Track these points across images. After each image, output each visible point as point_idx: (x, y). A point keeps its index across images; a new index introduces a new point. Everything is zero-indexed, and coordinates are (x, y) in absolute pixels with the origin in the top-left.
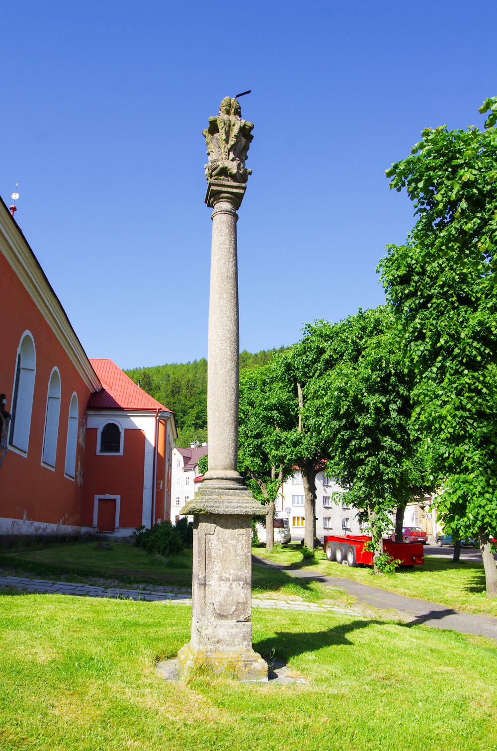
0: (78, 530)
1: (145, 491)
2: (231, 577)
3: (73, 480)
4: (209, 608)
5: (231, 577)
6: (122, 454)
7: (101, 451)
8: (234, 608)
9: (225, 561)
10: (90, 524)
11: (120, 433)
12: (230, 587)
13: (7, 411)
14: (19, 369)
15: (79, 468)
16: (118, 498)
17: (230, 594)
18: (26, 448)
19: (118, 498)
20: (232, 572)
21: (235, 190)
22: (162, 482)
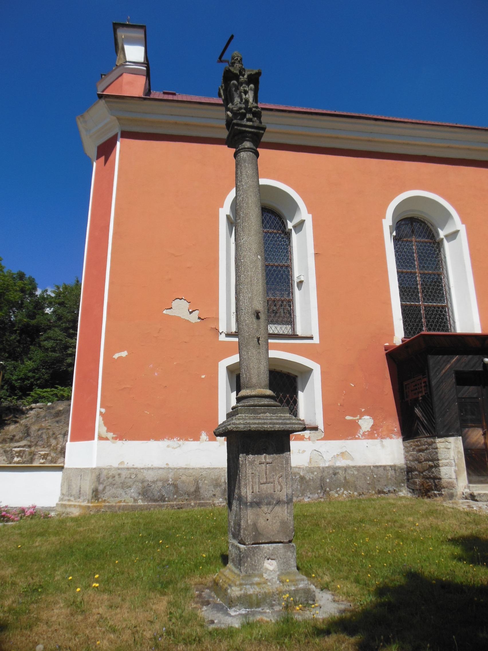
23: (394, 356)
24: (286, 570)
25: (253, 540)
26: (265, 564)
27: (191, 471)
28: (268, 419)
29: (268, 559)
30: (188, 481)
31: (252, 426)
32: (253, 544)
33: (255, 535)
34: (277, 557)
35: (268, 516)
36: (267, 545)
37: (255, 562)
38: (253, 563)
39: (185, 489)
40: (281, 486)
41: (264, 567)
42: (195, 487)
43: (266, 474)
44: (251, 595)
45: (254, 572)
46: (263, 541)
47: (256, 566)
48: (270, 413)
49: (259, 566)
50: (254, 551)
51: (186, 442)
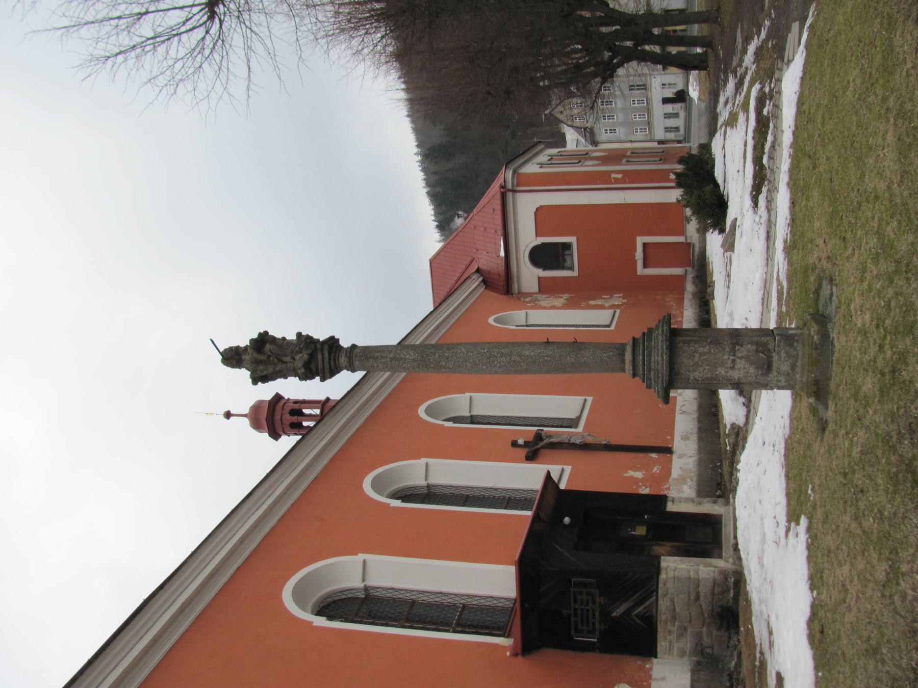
0: (690, 296)
1: (629, 201)
2: (732, 358)
3: (618, 311)
4: (761, 379)
5: (732, 358)
6: (575, 238)
7: (571, 268)
8: (761, 354)
9: (715, 363)
10: (682, 279)
11: (543, 244)
12: (741, 358)
13: (533, 435)
14: (473, 420)
15: (599, 302)
16: (640, 240)
17: (747, 358)
18: (580, 399)
19: (640, 240)
20: (726, 357)
21: (326, 355)
22: (613, 176)
23: (527, 647)
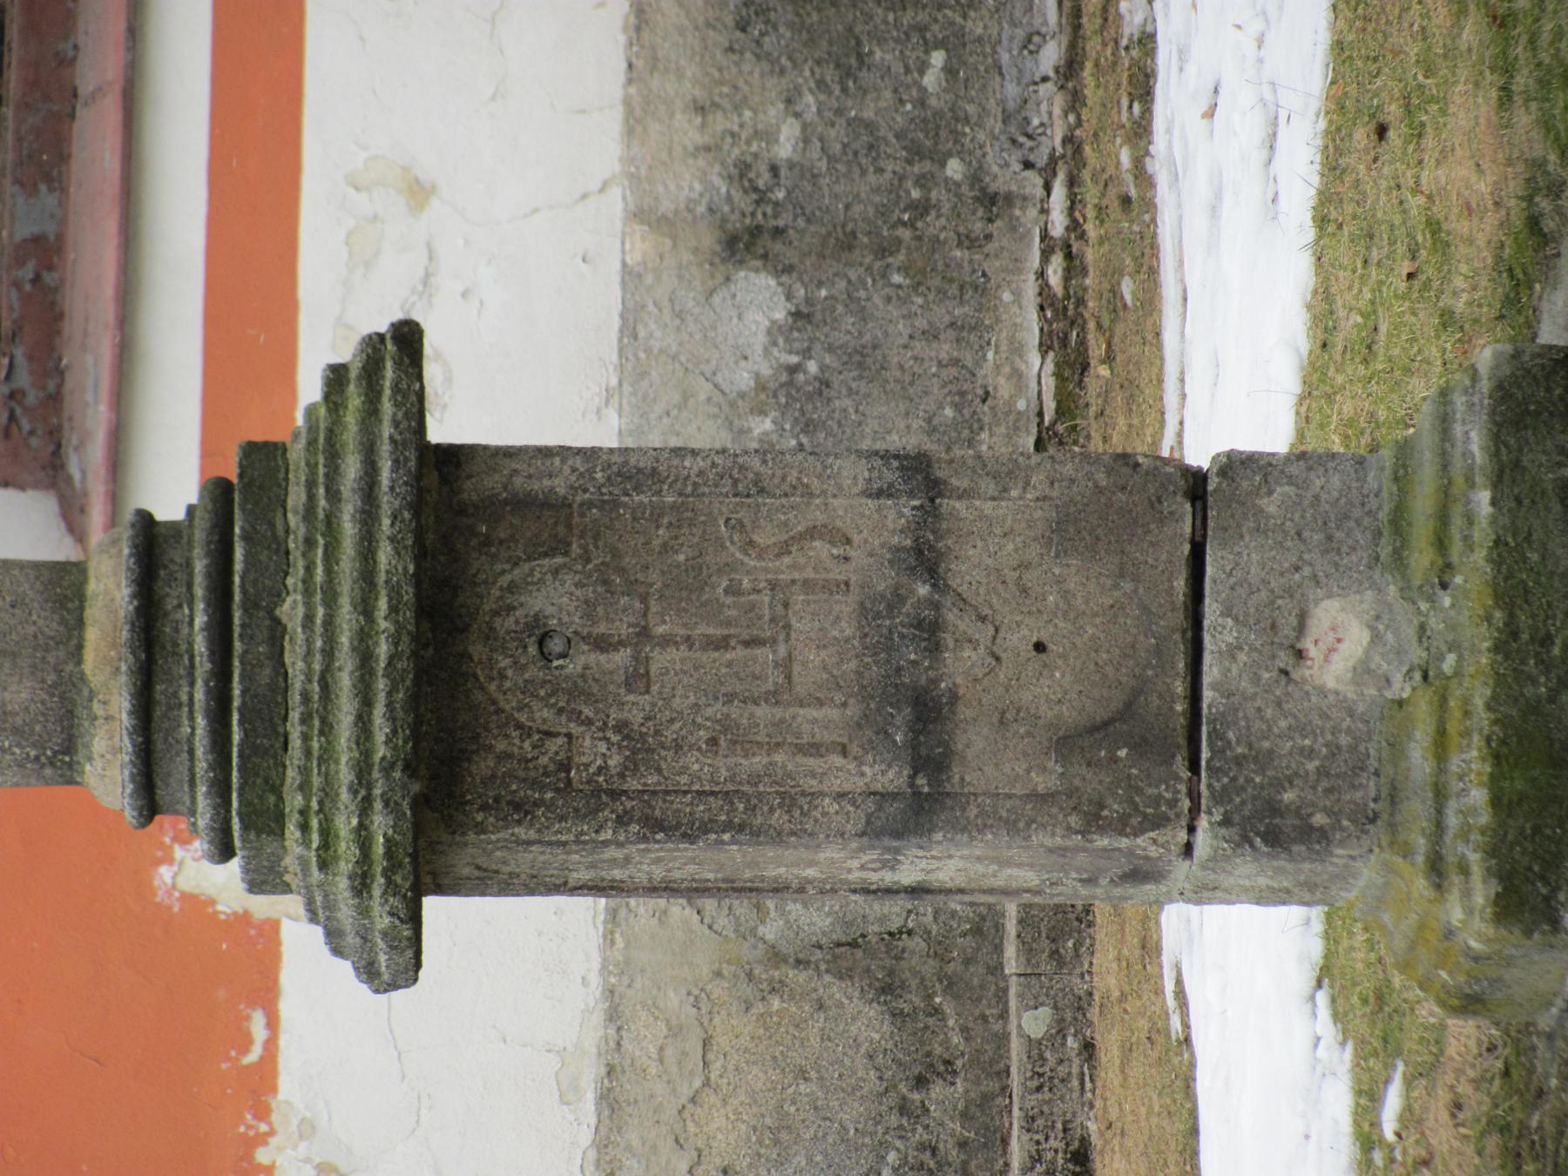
24: (1378, 534)
25: (1168, 761)
26: (1331, 683)
27: (645, 1040)
28: (329, 622)
29: (1300, 654)
30: (758, 1077)
31: (381, 751)
32: (1194, 766)
33: (1133, 747)
34: (1289, 592)
35: (1018, 640)
36: (1207, 659)
37: (1310, 753)
38: (1311, 766)
39: (851, 1114)
40: (812, 532)
41: (1350, 692)
42: (836, 990)
43: (721, 644)
44: (1496, 802)
45: (1373, 763)
46: (1180, 688)
47: (1335, 750)
48: (278, 595)
49: (1335, 731)
50: (1239, 761)
51: (291, 1090)
